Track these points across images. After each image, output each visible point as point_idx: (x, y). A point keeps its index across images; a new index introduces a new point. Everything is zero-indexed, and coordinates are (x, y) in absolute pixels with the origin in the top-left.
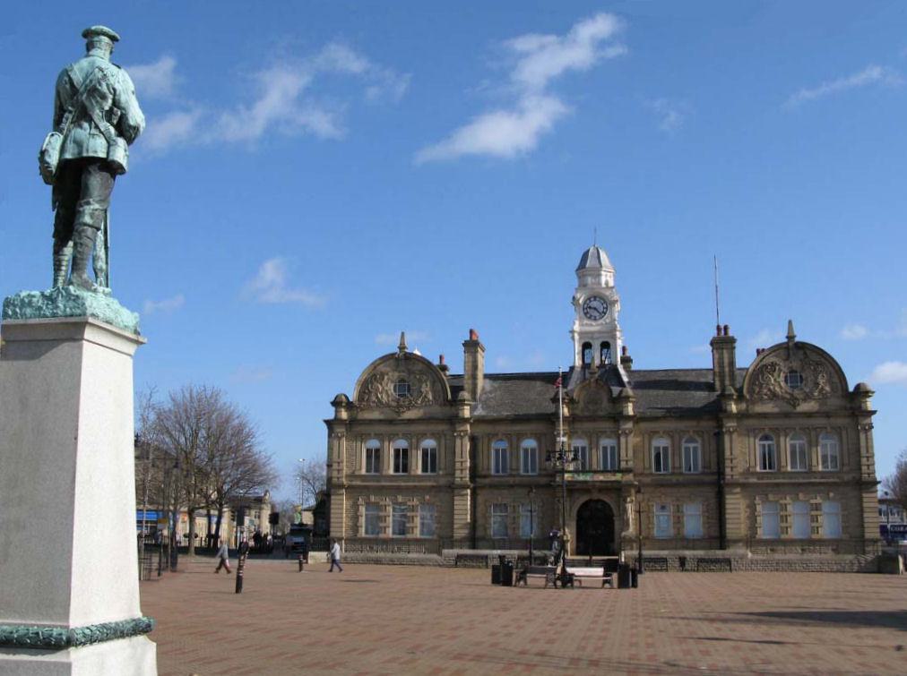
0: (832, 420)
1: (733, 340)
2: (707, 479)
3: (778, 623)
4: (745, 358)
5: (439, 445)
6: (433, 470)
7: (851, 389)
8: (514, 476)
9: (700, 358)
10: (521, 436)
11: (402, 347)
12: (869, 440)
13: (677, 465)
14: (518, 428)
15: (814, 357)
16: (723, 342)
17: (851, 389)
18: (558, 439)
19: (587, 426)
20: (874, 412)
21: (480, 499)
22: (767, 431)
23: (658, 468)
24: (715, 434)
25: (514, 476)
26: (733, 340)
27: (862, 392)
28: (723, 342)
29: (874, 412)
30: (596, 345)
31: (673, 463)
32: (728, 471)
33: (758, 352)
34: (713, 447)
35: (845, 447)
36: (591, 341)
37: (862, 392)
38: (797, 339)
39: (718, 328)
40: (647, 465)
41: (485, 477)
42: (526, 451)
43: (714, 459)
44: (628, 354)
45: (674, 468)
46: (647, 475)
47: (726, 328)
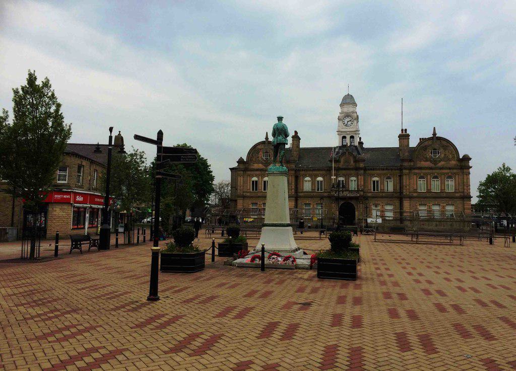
0: (451, 171)
1: (408, 135)
2: (395, 195)
3: (9, 266)
4: (413, 143)
5: (324, 180)
6: (256, 189)
7: (461, 157)
8: (382, 192)
9: (395, 143)
10: (317, 176)
11: (434, 134)
12: (468, 179)
13: (248, 188)
14: (348, 172)
15: (444, 143)
16: (404, 136)
17: (461, 157)
18: (332, 177)
19: (344, 172)
20: (471, 167)
21: (299, 202)
22: (450, 174)
23: (374, 190)
24: (399, 176)
25: (382, 192)
26: (408, 135)
27: (467, 159)
28: (404, 136)
29: (471, 167)
30: (348, 137)
31: (381, 187)
32: (404, 191)
33: (420, 139)
34: (398, 181)
35: (457, 183)
36: (346, 135)
37: (467, 159)
38: (437, 136)
39: (402, 130)
40: (248, 188)
41: (302, 192)
42: (318, 182)
43: (398, 187)
44: (362, 141)
45: (381, 190)
46: (248, 192)
47: (406, 130)
